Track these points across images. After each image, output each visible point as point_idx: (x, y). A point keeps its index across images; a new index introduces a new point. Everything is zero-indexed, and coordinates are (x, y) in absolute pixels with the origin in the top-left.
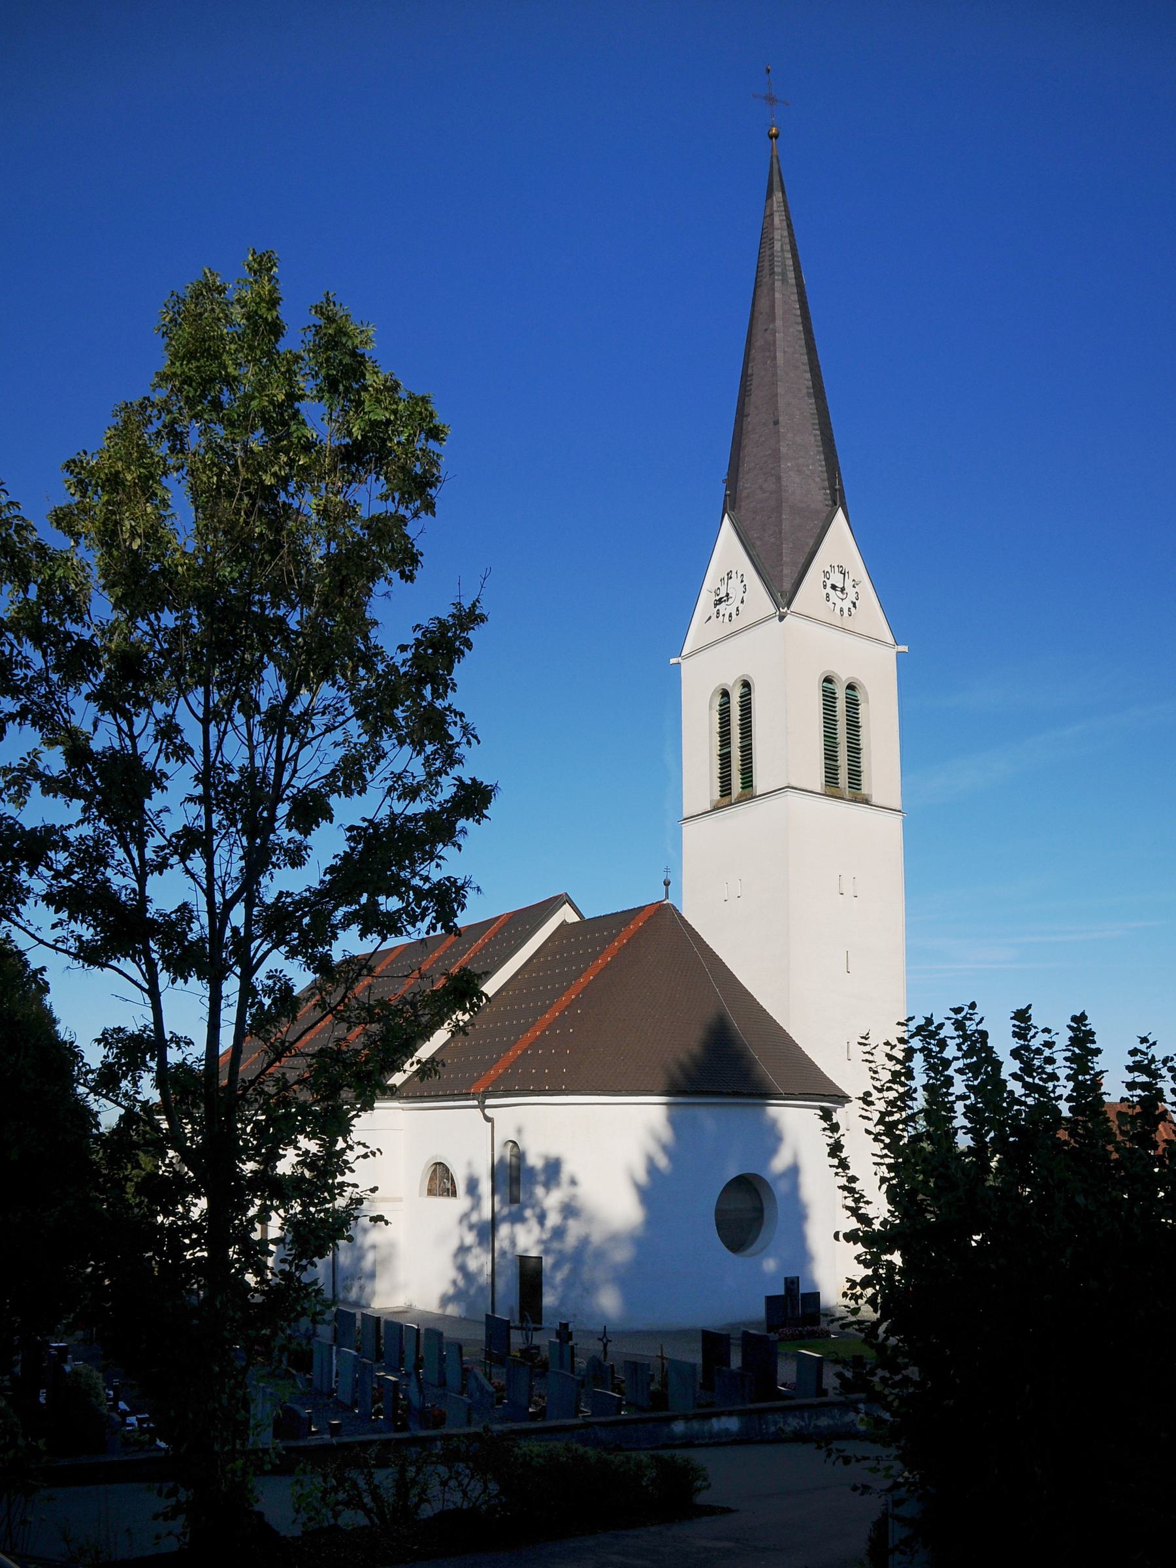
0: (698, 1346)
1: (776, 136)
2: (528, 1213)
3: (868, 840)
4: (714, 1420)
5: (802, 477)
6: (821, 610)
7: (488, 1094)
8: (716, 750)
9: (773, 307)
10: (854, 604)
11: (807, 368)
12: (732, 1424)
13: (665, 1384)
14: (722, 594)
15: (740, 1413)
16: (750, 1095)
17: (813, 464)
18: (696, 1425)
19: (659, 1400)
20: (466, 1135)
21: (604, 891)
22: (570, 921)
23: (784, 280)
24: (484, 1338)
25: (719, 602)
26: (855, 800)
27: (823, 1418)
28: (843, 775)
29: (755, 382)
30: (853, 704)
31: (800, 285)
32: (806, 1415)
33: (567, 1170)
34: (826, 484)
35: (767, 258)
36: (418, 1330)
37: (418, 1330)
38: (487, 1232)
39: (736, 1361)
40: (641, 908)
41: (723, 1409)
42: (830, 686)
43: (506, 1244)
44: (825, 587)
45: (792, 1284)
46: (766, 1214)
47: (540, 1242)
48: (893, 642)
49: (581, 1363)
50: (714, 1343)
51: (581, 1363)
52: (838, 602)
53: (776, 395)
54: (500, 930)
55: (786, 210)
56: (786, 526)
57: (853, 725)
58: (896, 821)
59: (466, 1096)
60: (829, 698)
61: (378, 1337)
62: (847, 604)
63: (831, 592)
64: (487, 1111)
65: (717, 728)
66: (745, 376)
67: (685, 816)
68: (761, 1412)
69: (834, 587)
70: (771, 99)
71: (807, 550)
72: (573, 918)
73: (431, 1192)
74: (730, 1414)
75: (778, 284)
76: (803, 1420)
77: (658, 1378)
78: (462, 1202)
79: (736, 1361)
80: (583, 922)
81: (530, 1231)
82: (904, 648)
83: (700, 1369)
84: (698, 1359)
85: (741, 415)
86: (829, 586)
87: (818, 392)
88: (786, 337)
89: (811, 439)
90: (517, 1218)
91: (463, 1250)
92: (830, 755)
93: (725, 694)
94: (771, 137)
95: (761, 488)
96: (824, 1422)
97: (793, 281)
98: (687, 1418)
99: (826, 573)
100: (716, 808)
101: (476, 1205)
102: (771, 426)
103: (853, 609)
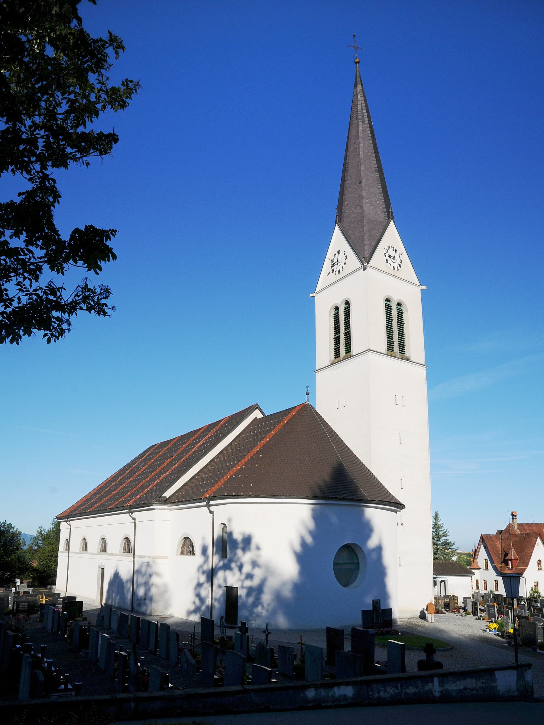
0: (325, 638)
1: (358, 63)
2: (233, 565)
3: (409, 379)
4: (336, 689)
5: (373, 206)
6: (384, 266)
7: (211, 498)
8: (333, 336)
9: (358, 133)
10: (400, 265)
11: (375, 159)
12: (348, 691)
13: (303, 661)
14: (335, 261)
15: (354, 684)
16: (352, 500)
17: (378, 201)
18: (323, 692)
19: (300, 673)
20: (200, 522)
21: (276, 401)
22: (258, 417)
23: (363, 122)
24: (200, 632)
25: (333, 265)
26: (402, 358)
27: (410, 687)
28: (396, 345)
29: (350, 166)
30: (400, 314)
31: (370, 124)
32: (399, 685)
33: (255, 541)
34: (385, 210)
35: (355, 113)
36: (157, 624)
37: (157, 624)
38: (211, 575)
39: (348, 647)
40: (295, 407)
41: (341, 681)
42: (389, 303)
43: (221, 582)
44: (385, 256)
45: (376, 604)
46: (361, 565)
47: (239, 580)
48: (419, 284)
49: (253, 647)
50: (334, 636)
51: (253, 647)
52: (392, 263)
53: (360, 170)
54: (225, 424)
55: (363, 93)
56: (366, 228)
57: (401, 323)
58: (422, 372)
59: (200, 500)
60: (388, 308)
61: (138, 628)
62: (396, 265)
63: (389, 258)
64: (211, 508)
65: (333, 325)
66: (345, 164)
67: (317, 368)
68: (368, 683)
69: (390, 256)
70: (356, 48)
71: (376, 239)
72: (260, 416)
73: (182, 553)
74: (347, 684)
75: (360, 123)
76: (397, 689)
77: (299, 657)
78: (198, 559)
79: (348, 647)
80: (265, 417)
81: (234, 575)
82: (424, 287)
83: (325, 651)
84: (324, 646)
85: (343, 180)
86: (387, 255)
87: (380, 169)
88: (364, 146)
89: (377, 190)
90: (227, 567)
91: (199, 585)
92: (390, 336)
93: (337, 308)
94: (356, 63)
95: (353, 212)
96: (411, 690)
97: (367, 122)
98: (317, 687)
99: (386, 250)
100: (332, 364)
101: (206, 561)
102: (358, 184)
103: (399, 267)
